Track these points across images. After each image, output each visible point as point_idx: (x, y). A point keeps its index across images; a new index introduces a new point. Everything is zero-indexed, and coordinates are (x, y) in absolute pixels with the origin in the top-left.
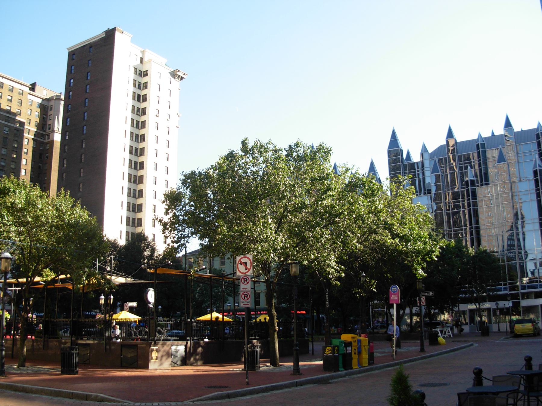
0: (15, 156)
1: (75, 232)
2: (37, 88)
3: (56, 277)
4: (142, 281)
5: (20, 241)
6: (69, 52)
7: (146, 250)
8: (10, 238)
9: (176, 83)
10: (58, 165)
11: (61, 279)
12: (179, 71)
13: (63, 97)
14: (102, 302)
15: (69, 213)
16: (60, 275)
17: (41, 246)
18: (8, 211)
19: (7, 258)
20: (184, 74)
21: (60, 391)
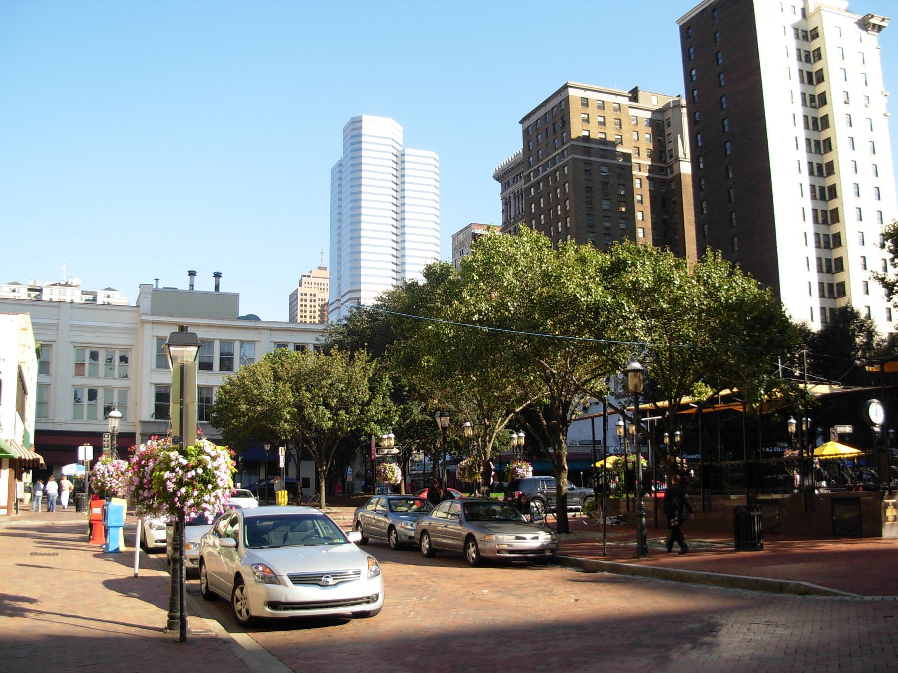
0: (623, 210)
1: (739, 316)
2: (641, 95)
3: (715, 394)
4: (859, 389)
5: (653, 341)
6: (681, 27)
7: (857, 336)
8: (635, 339)
9: (871, 39)
10: (693, 212)
11: (723, 397)
12: (872, 17)
13: (684, 102)
14: (792, 429)
15: (726, 287)
16: (721, 390)
17: (686, 346)
18: (629, 296)
19: (636, 371)
20: (883, 20)
21: (736, 578)
